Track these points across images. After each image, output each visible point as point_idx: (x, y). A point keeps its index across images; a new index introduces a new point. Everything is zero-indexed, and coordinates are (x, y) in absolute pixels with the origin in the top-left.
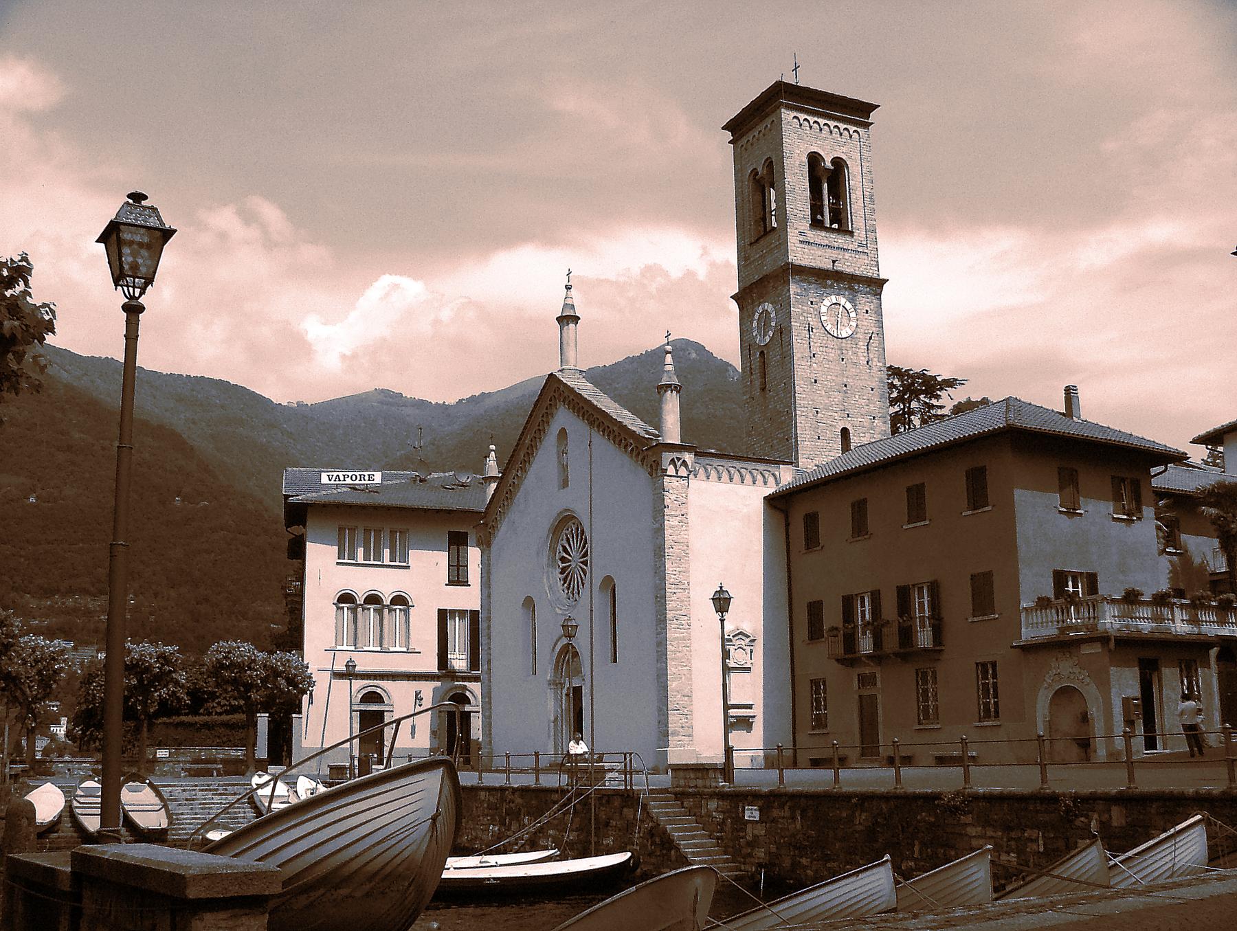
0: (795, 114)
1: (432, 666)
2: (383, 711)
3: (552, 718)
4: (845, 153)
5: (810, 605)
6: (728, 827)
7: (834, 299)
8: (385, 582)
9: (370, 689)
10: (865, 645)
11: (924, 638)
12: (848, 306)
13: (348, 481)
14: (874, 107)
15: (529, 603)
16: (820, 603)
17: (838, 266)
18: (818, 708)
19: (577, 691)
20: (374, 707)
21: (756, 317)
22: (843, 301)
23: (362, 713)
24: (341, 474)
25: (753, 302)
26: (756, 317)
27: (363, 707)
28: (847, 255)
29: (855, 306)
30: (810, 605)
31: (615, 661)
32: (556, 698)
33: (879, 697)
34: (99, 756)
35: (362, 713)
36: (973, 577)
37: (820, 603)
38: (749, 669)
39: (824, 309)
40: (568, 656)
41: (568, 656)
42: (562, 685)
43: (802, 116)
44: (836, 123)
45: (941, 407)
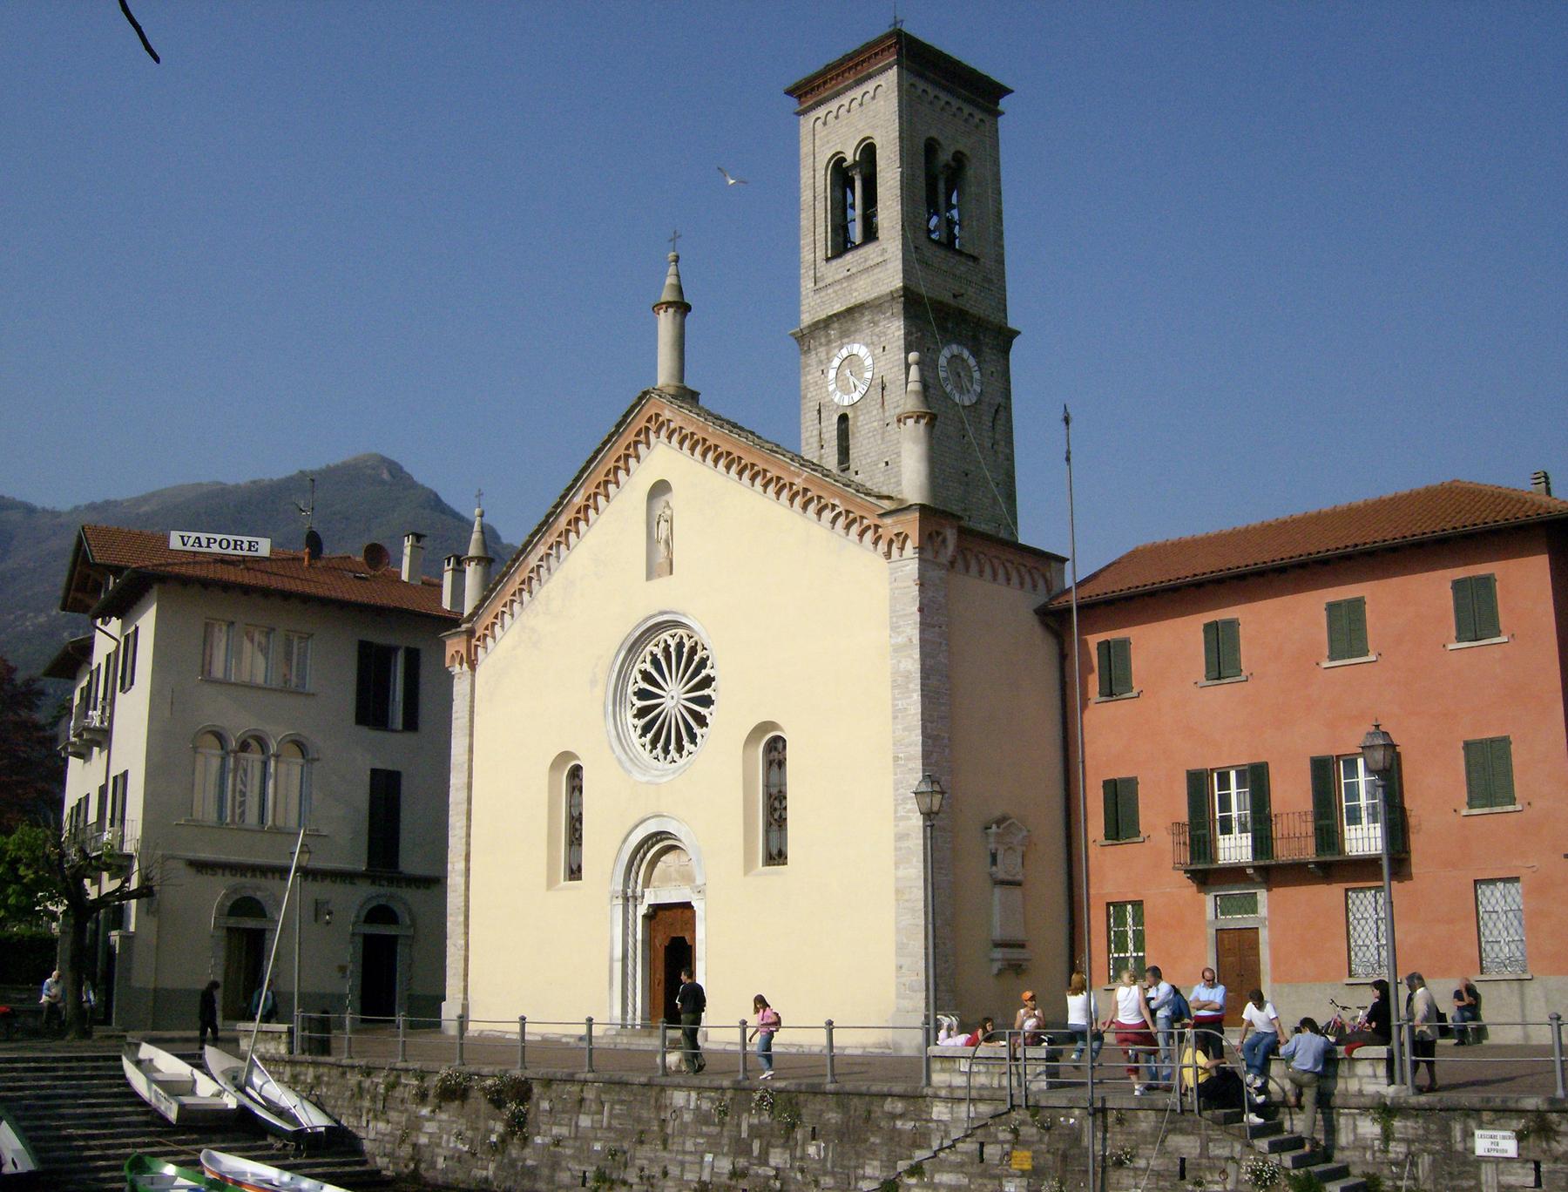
6: (1028, 1132)
7: (955, 349)
10: (1235, 848)
11: (1364, 839)
12: (972, 362)
13: (215, 548)
14: (1003, 91)
16: (1131, 783)
17: (961, 303)
18: (1118, 950)
20: (251, 923)
21: (836, 363)
22: (966, 354)
24: (203, 536)
25: (829, 342)
26: (836, 363)
27: (233, 922)
29: (978, 363)
31: (776, 856)
33: (1264, 935)
36: (1468, 746)
37: (1131, 783)
38: (1018, 884)
39: (942, 361)
45: (902, 549)
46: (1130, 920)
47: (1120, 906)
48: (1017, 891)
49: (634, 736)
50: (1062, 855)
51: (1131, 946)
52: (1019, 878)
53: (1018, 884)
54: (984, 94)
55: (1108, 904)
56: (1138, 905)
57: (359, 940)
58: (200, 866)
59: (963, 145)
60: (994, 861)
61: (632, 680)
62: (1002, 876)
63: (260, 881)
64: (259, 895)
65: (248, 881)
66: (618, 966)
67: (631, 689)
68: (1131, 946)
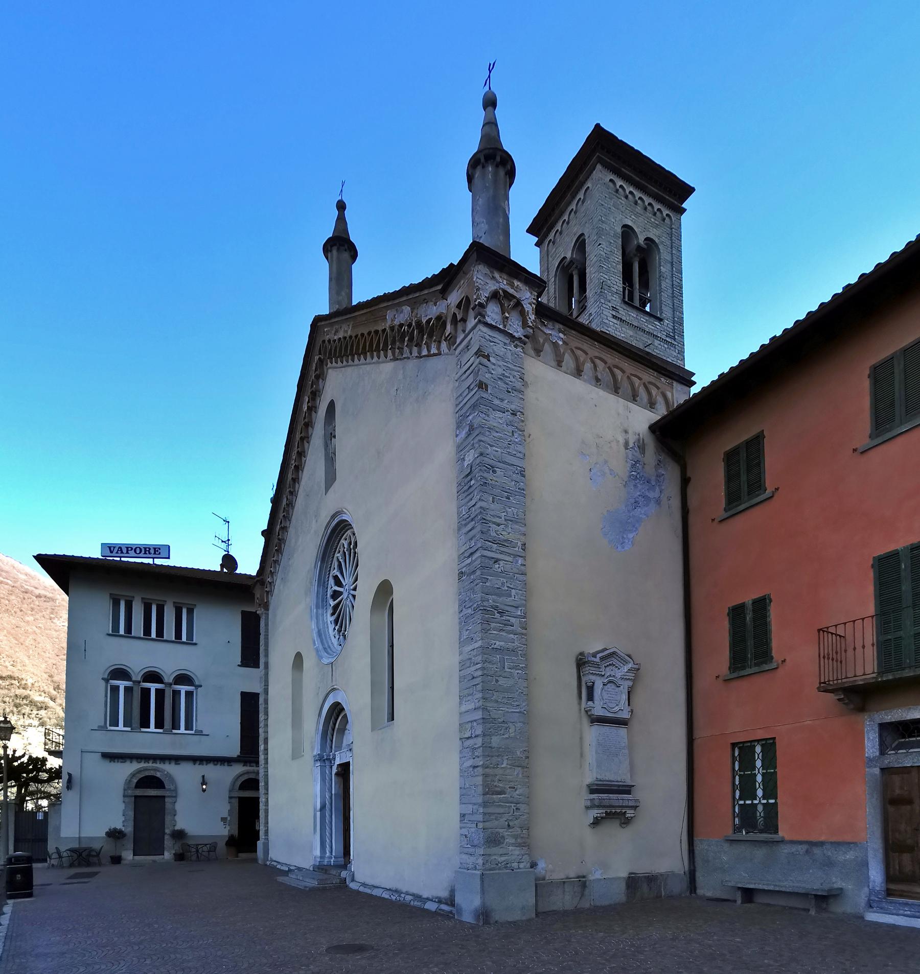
0: (612, 177)
1: (233, 748)
2: (164, 797)
3: (319, 807)
4: (659, 237)
5: (737, 612)
8: (167, 659)
9: (147, 773)
15: (299, 657)
19: (344, 771)
23: (241, 799)
27: (139, 792)
28: (657, 342)
30: (737, 612)
32: (323, 779)
34: (93, 814)
35: (241, 799)
38: (622, 723)
40: (336, 716)
41: (336, 716)
42: (331, 761)
43: (619, 182)
44: (651, 200)
46: (759, 764)
47: (744, 750)
48: (622, 731)
49: (331, 627)
50: (694, 581)
51: (760, 793)
52: (625, 715)
53: (622, 723)
54: (671, 192)
55: (734, 745)
56: (769, 746)
57: (236, 802)
58: (110, 757)
59: (653, 234)
60: (590, 697)
61: (329, 587)
62: (598, 711)
63: (158, 765)
64: (158, 775)
65: (150, 764)
66: (318, 814)
67: (329, 593)
68: (760, 793)
